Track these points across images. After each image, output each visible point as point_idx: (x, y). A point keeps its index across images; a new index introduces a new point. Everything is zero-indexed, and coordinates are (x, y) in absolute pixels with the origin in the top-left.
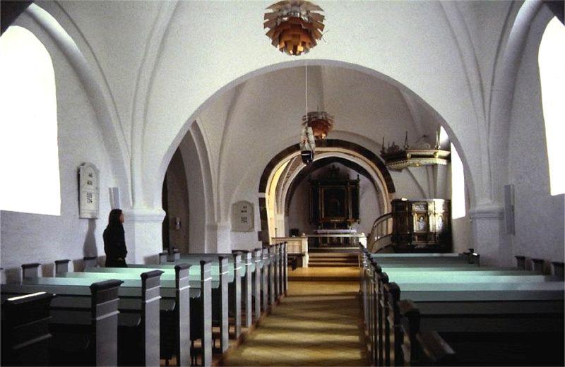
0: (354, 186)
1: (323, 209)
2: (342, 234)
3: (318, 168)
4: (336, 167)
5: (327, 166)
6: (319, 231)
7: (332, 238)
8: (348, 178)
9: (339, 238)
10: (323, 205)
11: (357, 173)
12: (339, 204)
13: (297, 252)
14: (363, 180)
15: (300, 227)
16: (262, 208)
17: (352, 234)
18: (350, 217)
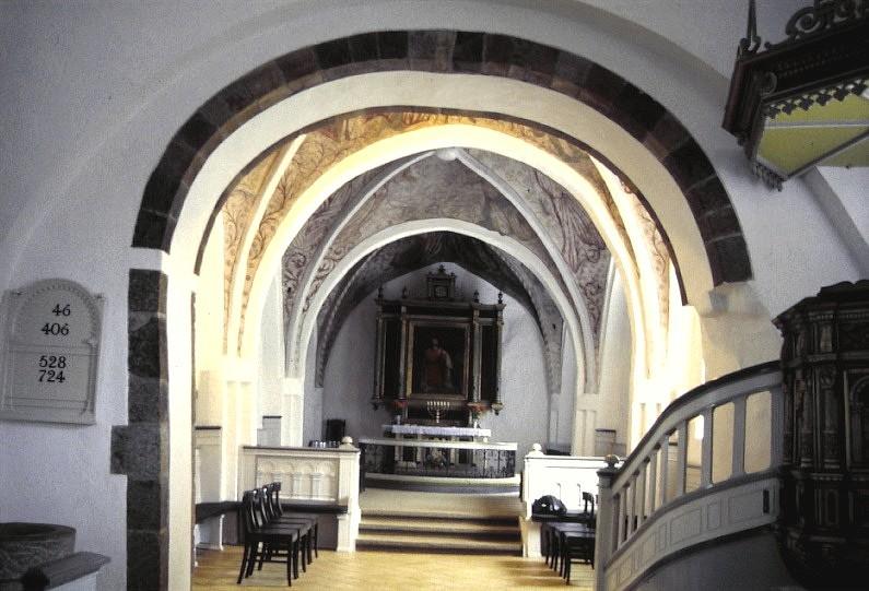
0: (490, 320)
1: (410, 373)
2: (451, 440)
3: (400, 274)
4: (448, 272)
5: (425, 270)
6: (397, 429)
7: (428, 450)
8: (477, 301)
9: (446, 452)
10: (410, 365)
11: (498, 291)
12: (449, 362)
13: (322, 496)
14: (513, 309)
15: (351, 415)
16: (144, 318)
17: (480, 439)
18: (477, 395)
